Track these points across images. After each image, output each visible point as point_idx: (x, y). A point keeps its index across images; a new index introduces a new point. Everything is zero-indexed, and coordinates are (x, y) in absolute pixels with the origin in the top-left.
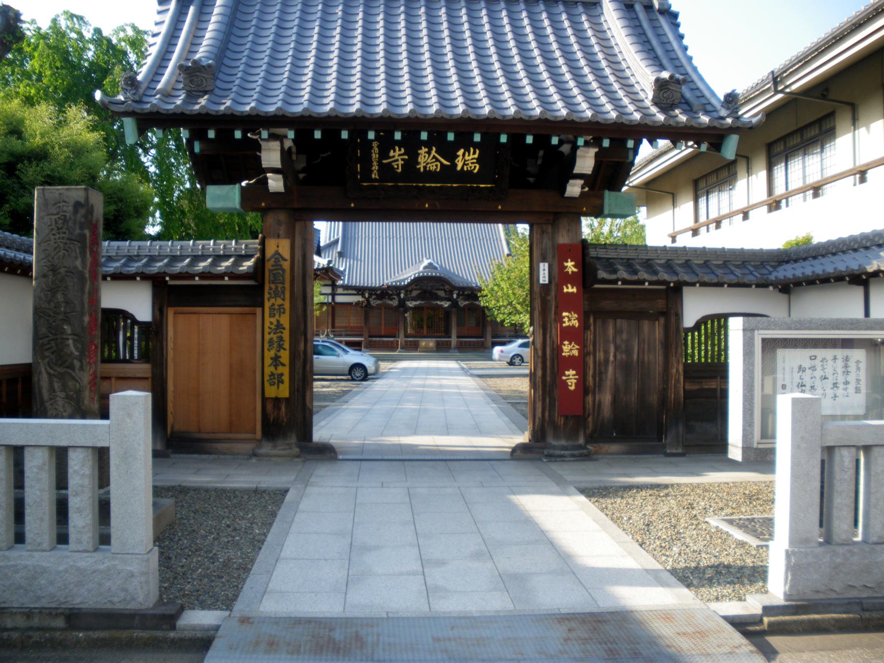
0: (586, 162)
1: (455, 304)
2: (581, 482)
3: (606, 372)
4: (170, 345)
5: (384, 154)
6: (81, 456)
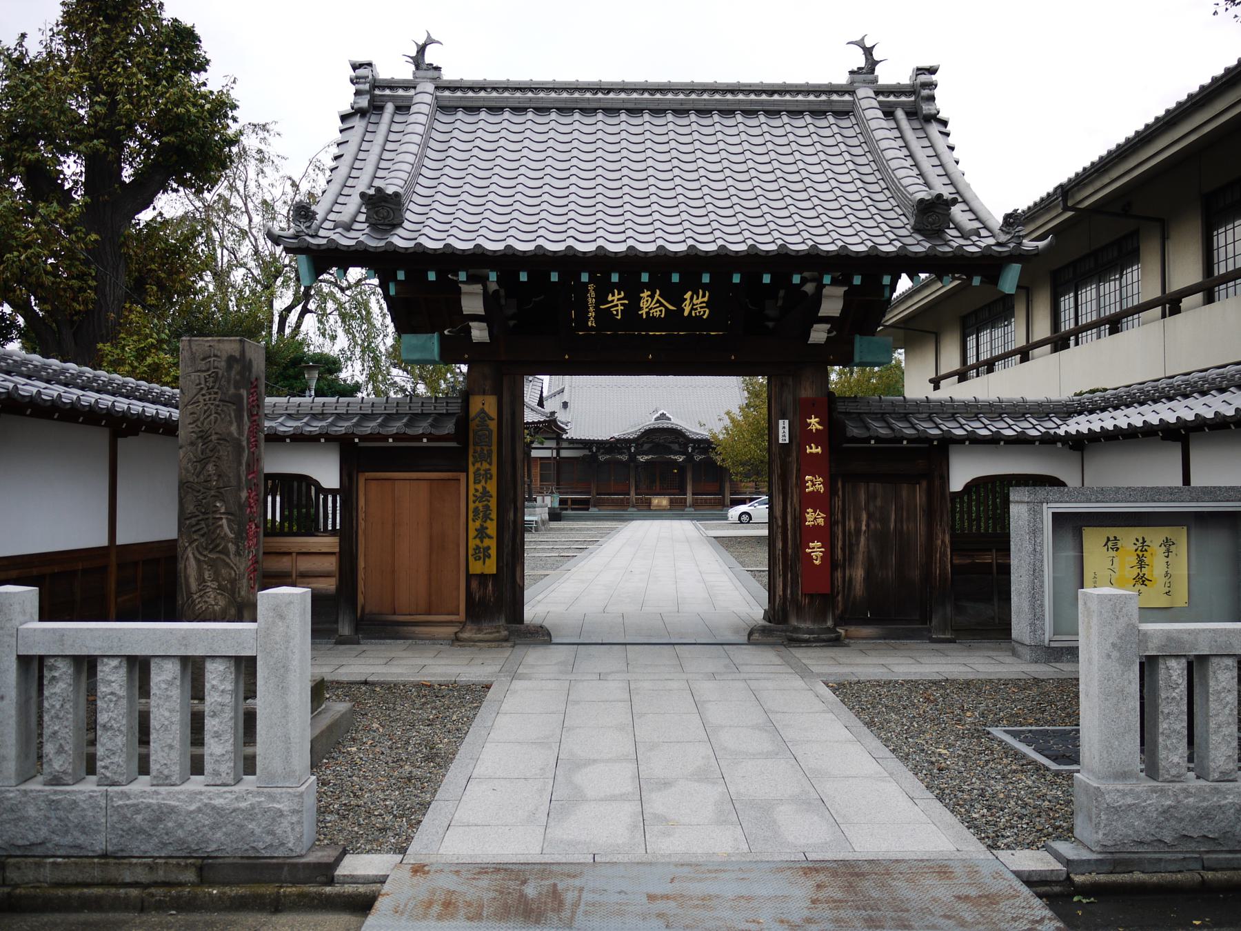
0: (832, 306)
1: (690, 458)
2: (830, 674)
3: (858, 544)
4: (361, 515)
5: (601, 299)
6: (221, 668)
